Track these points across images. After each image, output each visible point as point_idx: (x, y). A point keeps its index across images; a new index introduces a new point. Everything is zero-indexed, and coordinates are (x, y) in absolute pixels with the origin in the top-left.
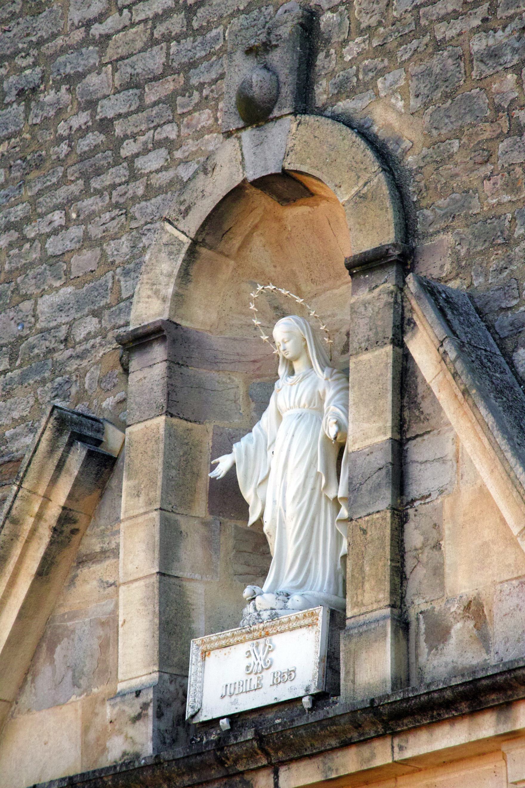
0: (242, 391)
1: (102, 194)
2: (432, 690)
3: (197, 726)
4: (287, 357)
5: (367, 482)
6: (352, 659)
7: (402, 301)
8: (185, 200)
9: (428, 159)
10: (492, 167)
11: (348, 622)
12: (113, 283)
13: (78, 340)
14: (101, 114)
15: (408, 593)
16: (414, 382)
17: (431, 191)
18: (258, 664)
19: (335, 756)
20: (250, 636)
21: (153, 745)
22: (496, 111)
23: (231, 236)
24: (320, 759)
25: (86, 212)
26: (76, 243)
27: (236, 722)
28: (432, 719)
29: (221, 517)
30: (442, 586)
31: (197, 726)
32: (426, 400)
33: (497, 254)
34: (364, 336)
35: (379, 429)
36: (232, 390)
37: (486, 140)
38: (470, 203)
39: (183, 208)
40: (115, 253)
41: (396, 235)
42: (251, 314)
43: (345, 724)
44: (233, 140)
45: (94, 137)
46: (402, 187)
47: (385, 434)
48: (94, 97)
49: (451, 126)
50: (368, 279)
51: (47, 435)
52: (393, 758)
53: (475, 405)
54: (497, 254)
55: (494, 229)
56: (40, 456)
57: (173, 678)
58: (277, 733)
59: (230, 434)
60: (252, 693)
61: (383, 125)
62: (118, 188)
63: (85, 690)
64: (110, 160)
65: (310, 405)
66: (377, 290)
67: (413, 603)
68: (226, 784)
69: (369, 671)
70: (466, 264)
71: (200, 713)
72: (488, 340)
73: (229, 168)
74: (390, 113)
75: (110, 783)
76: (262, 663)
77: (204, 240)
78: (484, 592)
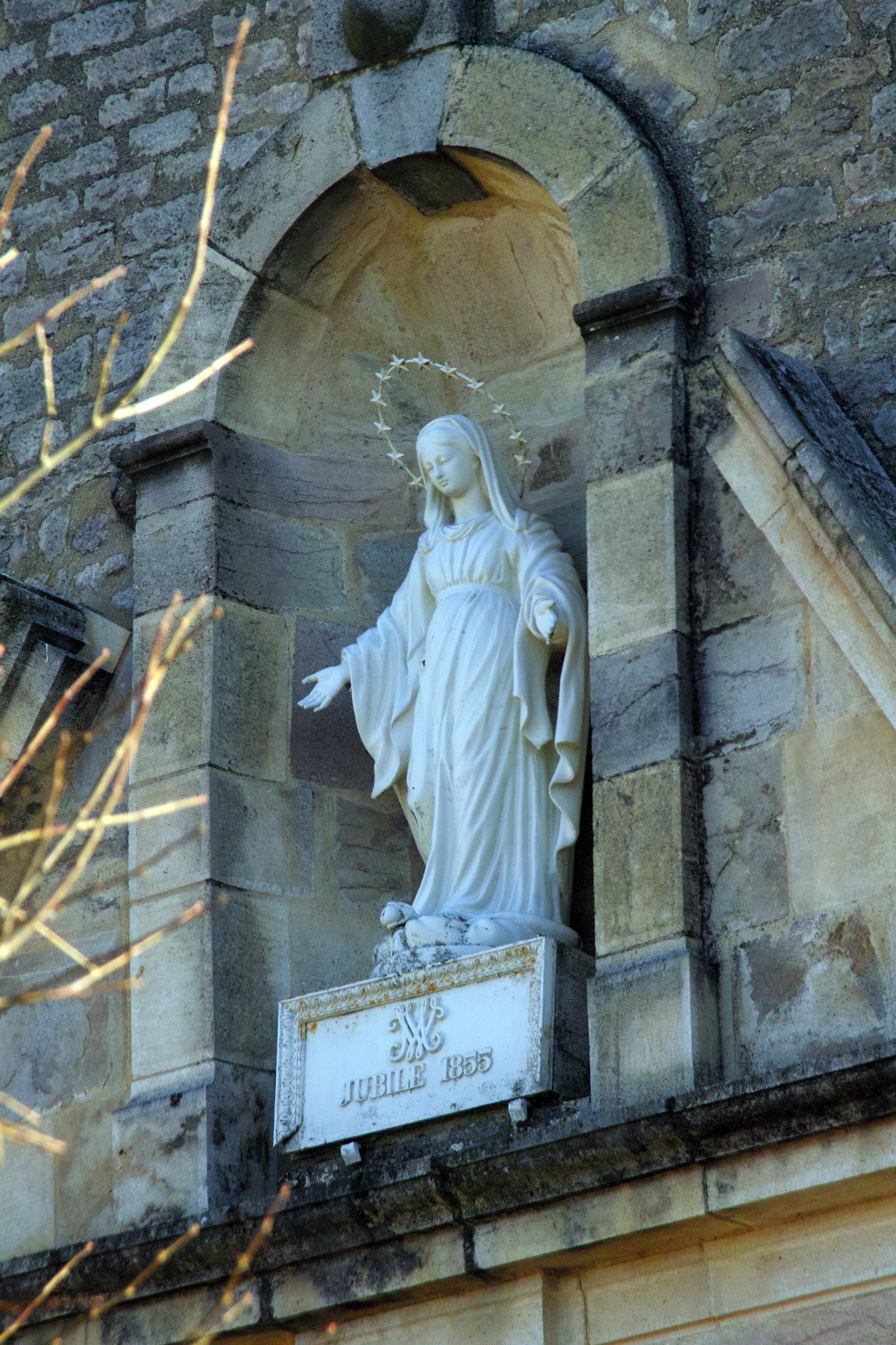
0: (345, 555)
1: (65, 194)
2: (791, 1080)
3: (292, 1158)
4: (444, 490)
5: (630, 710)
6: (612, 1031)
7: (686, 384)
8: (240, 203)
9: (728, 125)
10: (860, 138)
11: (599, 964)
12: (92, 356)
13: (21, 461)
14: (56, 48)
15: (714, 910)
16: (713, 529)
17: (736, 184)
18: (416, 1043)
19: (588, 1206)
20: (399, 992)
21: (209, 1193)
22: (863, 37)
23: (325, 271)
24: (559, 1211)
25: (32, 228)
26: (13, 284)
27: (372, 1149)
28: (787, 1135)
29: (313, 783)
30: (784, 896)
31: (292, 1158)
32: (739, 561)
33: (873, 296)
34: (615, 447)
35: (652, 614)
36: (328, 554)
37: (847, 88)
38: (816, 203)
39: (236, 217)
40: (95, 301)
41: (673, 263)
42: (373, 412)
43: (614, 1145)
44: (334, 94)
45: (43, 90)
46: (678, 177)
47: (663, 623)
48: (41, 17)
49: (774, 64)
50: (619, 343)
52: (707, 1207)
53: (864, 563)
54: (873, 296)
55: (867, 250)
57: (239, 1072)
58: (477, 1163)
59: (326, 632)
60: (404, 1097)
61: (634, 66)
62: (98, 184)
63: (60, 1097)
64: (79, 132)
65: (490, 576)
66: (637, 364)
67: (725, 928)
68: (365, 1259)
69: (648, 1051)
70: (811, 315)
71: (300, 1134)
72: (863, 451)
73: (329, 143)
74: (647, 42)
75: (135, 1260)
76: (423, 1041)
77: (277, 276)
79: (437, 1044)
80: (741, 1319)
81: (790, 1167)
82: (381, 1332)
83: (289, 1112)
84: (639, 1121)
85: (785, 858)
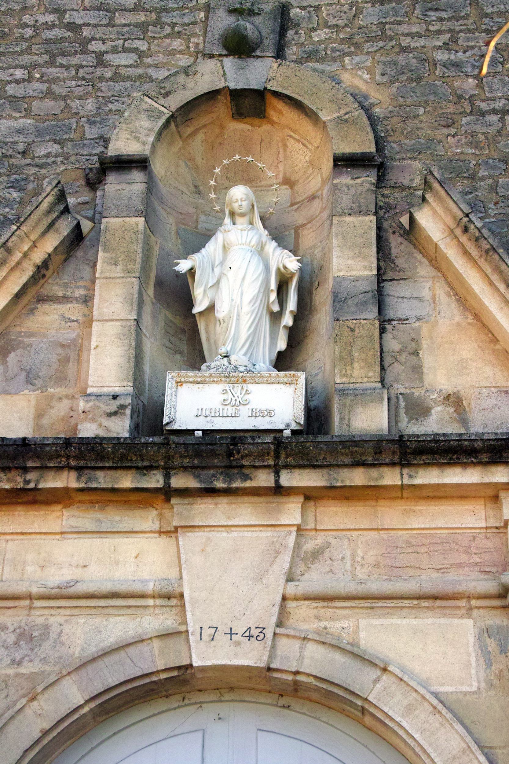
0: (173, 229)
5: (354, 298)
6: (347, 411)
13: (36, 155)
20: (228, 380)
24: (325, 470)
37: (450, 113)
38: (435, 147)
39: (163, 91)
47: (371, 271)
51: (50, 199)
52: (402, 482)
56: (41, 211)
66: (359, 181)
75: (110, 449)
78: (463, 391)
79: (246, 403)
80: (390, 532)
81: (445, 474)
82: (216, 504)
83: (170, 413)
84: (383, 441)
85: (422, 366)
